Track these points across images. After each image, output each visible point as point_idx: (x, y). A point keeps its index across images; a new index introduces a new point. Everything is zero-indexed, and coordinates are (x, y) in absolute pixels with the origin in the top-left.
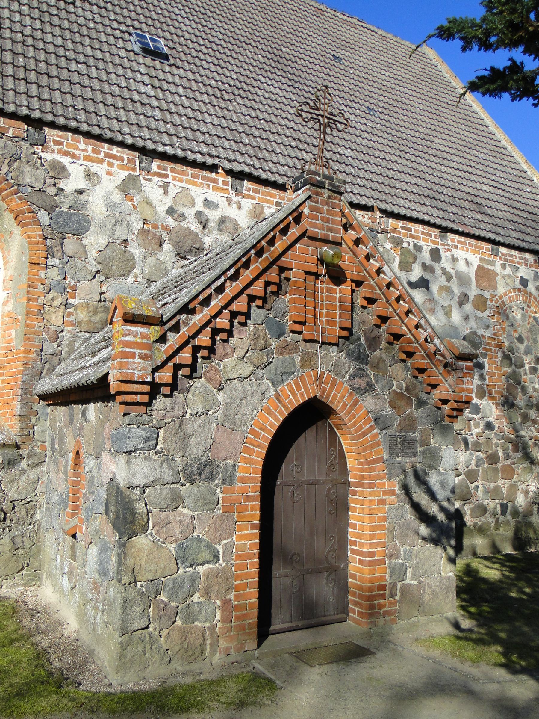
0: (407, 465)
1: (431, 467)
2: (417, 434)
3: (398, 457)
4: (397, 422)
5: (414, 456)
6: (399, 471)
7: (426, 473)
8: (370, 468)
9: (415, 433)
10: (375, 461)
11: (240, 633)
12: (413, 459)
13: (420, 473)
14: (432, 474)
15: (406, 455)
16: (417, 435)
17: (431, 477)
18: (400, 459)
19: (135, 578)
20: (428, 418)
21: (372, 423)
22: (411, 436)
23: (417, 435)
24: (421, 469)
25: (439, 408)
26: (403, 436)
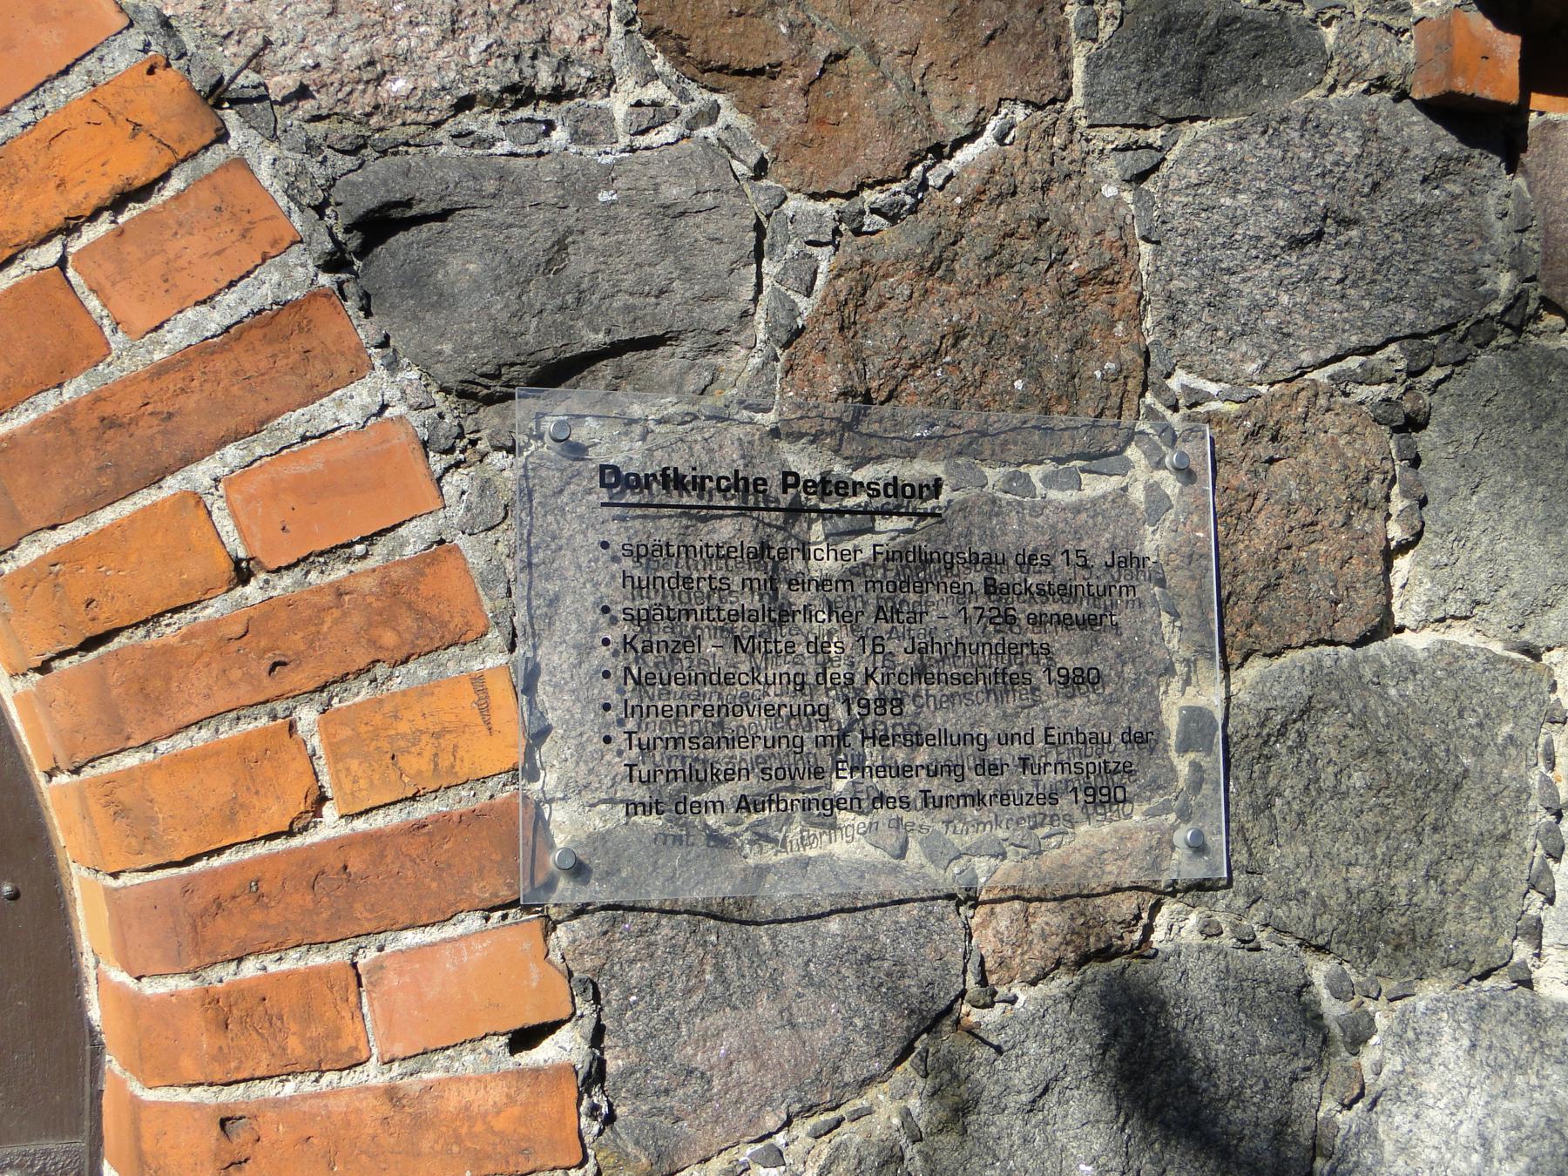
0: (992, 932)
1: (1392, 940)
2: (1141, 474)
3: (825, 812)
4: (798, 281)
5: (1104, 795)
6: (838, 1023)
7: (1311, 1034)
8: (222, 1011)
9: (1100, 458)
10: (345, 894)
11: (628, 563)
12: (1091, 842)
13: (1216, 1034)
14: (1408, 1038)
15: (969, 779)
16: (1144, 496)
17: (1405, 1090)
18: (850, 844)
19: (561, 245)
20: (1330, 260)
21: (297, 273)
22: (1051, 499)
23: (1144, 496)
24: (1239, 989)
25: (1492, 129)
26: (900, 497)
